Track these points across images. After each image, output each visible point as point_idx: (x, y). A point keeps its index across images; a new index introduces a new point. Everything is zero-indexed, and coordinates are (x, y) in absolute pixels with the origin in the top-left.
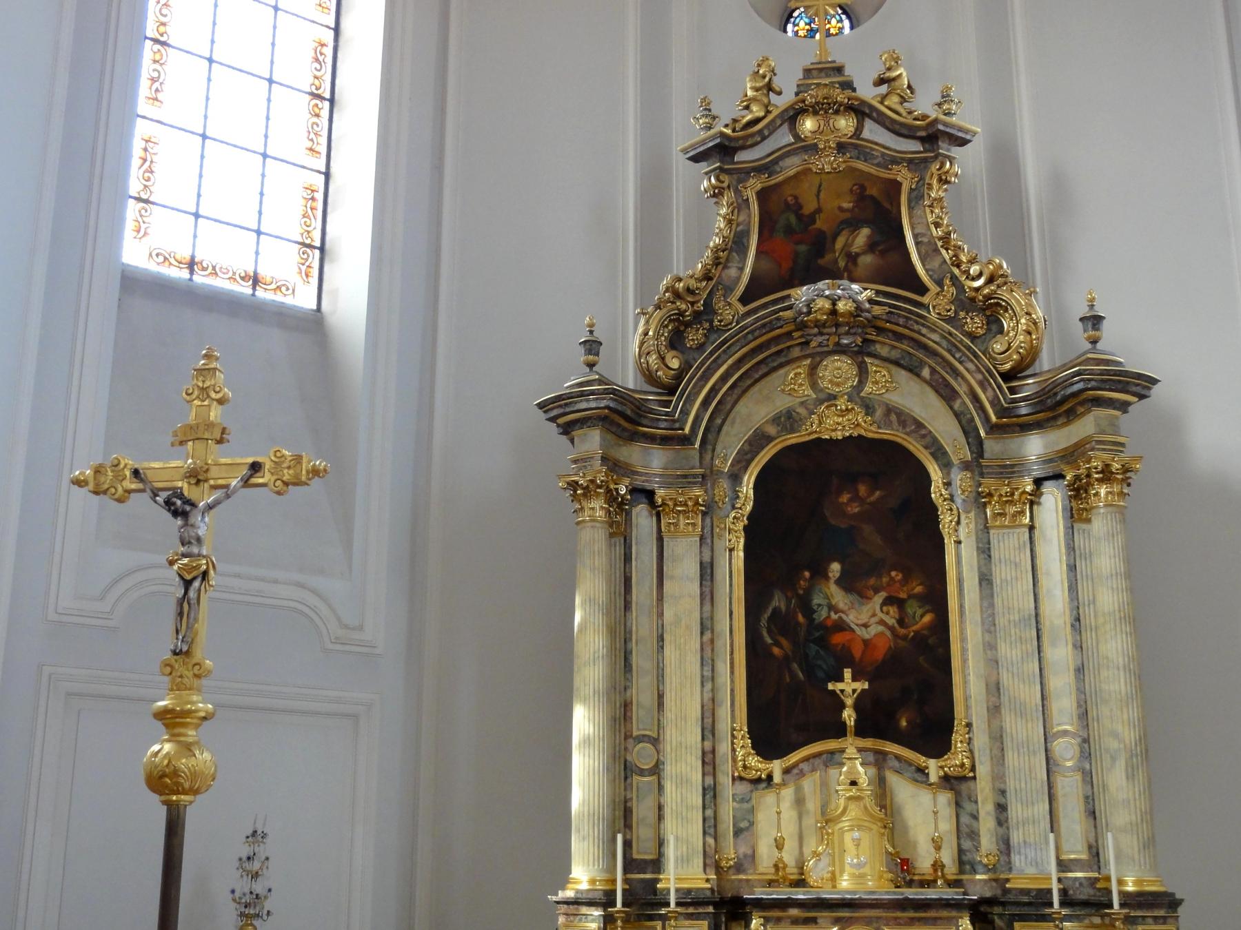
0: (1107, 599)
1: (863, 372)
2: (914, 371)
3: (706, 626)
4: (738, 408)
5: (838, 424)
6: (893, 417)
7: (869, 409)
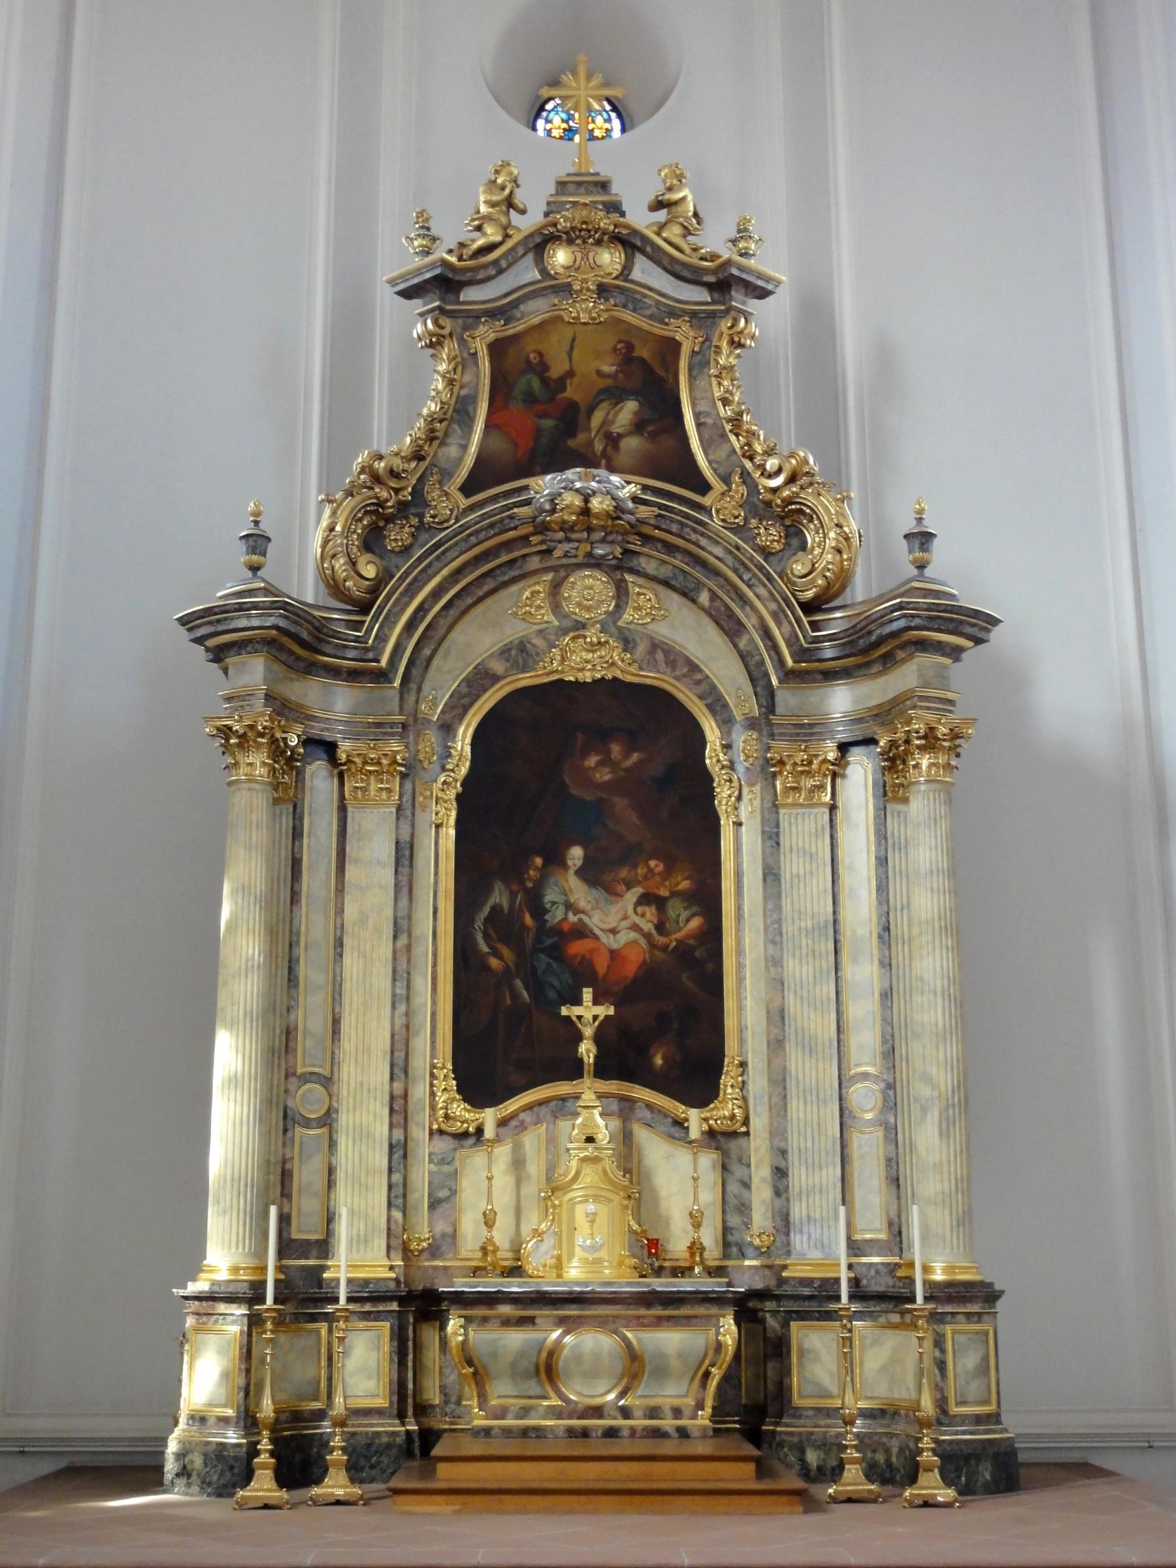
0: (925, 902)
1: (621, 592)
2: (689, 595)
3: (401, 927)
4: (453, 635)
5: (587, 661)
6: (660, 656)
7: (627, 643)
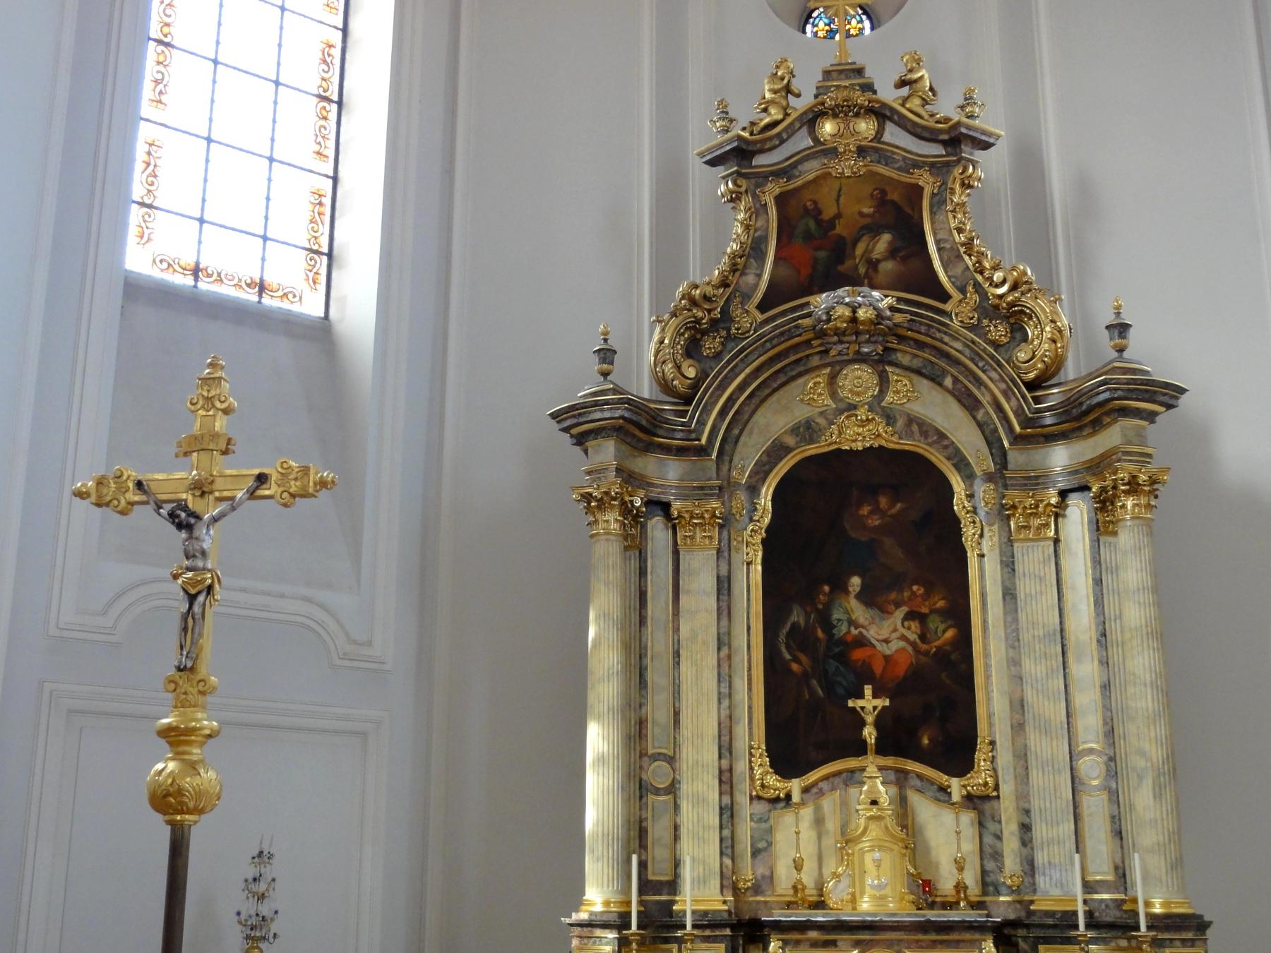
0: (1134, 613)
1: (884, 381)
2: (936, 380)
3: (723, 641)
4: (756, 418)
5: (858, 434)
6: (915, 428)
7: (890, 419)
